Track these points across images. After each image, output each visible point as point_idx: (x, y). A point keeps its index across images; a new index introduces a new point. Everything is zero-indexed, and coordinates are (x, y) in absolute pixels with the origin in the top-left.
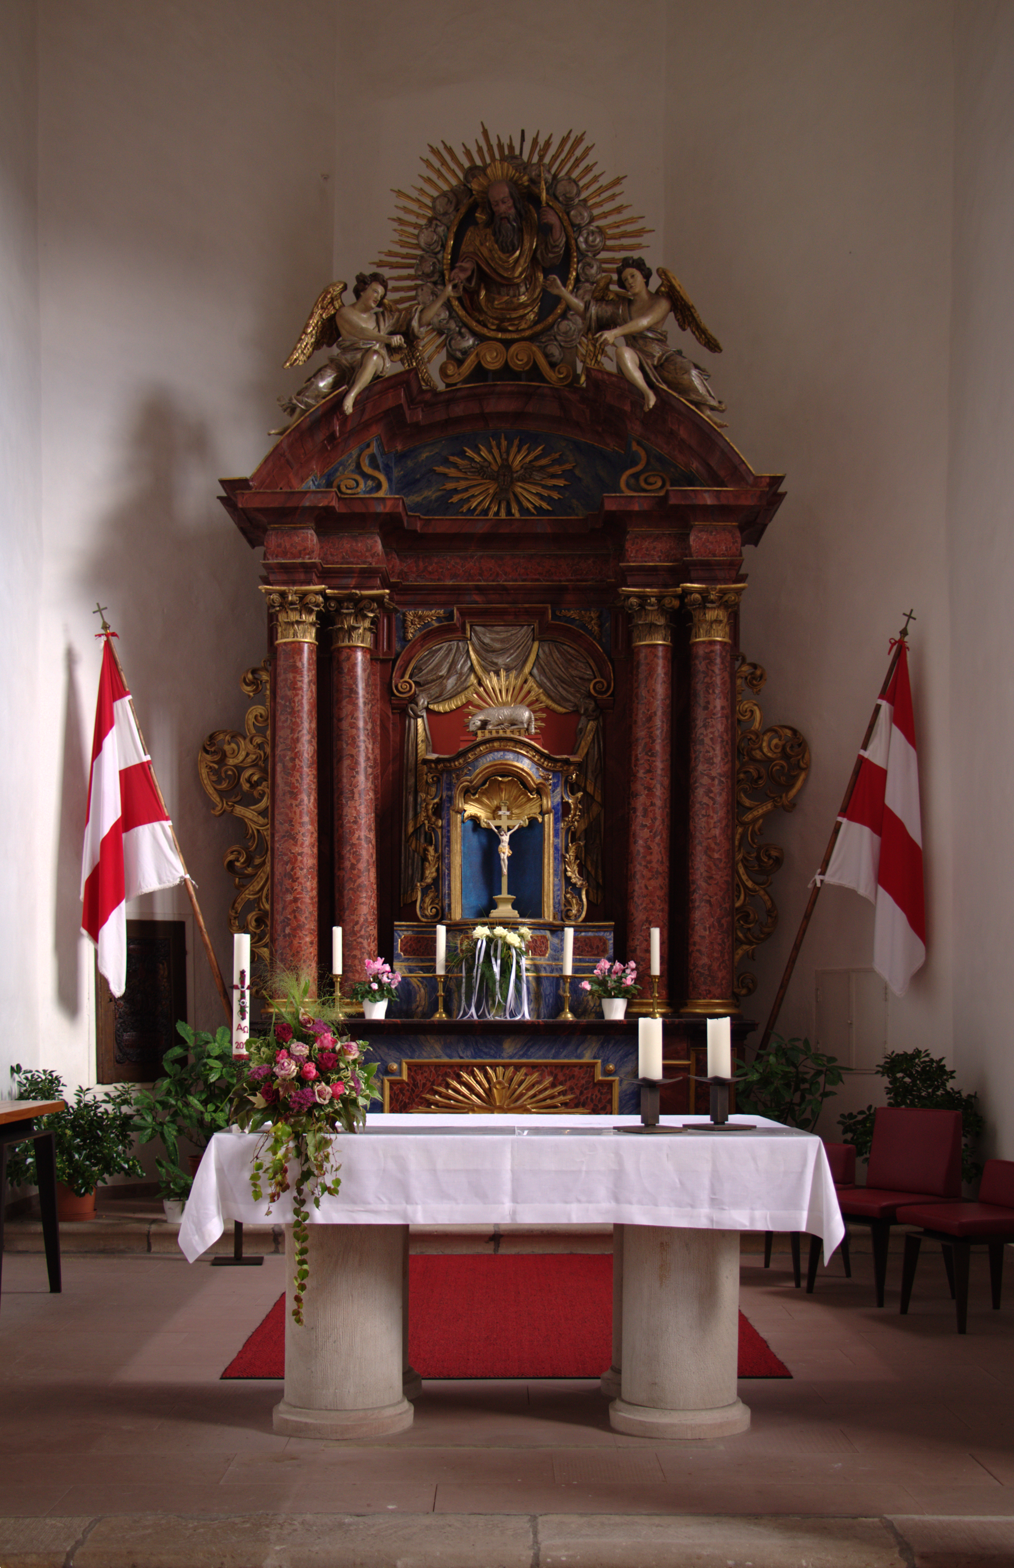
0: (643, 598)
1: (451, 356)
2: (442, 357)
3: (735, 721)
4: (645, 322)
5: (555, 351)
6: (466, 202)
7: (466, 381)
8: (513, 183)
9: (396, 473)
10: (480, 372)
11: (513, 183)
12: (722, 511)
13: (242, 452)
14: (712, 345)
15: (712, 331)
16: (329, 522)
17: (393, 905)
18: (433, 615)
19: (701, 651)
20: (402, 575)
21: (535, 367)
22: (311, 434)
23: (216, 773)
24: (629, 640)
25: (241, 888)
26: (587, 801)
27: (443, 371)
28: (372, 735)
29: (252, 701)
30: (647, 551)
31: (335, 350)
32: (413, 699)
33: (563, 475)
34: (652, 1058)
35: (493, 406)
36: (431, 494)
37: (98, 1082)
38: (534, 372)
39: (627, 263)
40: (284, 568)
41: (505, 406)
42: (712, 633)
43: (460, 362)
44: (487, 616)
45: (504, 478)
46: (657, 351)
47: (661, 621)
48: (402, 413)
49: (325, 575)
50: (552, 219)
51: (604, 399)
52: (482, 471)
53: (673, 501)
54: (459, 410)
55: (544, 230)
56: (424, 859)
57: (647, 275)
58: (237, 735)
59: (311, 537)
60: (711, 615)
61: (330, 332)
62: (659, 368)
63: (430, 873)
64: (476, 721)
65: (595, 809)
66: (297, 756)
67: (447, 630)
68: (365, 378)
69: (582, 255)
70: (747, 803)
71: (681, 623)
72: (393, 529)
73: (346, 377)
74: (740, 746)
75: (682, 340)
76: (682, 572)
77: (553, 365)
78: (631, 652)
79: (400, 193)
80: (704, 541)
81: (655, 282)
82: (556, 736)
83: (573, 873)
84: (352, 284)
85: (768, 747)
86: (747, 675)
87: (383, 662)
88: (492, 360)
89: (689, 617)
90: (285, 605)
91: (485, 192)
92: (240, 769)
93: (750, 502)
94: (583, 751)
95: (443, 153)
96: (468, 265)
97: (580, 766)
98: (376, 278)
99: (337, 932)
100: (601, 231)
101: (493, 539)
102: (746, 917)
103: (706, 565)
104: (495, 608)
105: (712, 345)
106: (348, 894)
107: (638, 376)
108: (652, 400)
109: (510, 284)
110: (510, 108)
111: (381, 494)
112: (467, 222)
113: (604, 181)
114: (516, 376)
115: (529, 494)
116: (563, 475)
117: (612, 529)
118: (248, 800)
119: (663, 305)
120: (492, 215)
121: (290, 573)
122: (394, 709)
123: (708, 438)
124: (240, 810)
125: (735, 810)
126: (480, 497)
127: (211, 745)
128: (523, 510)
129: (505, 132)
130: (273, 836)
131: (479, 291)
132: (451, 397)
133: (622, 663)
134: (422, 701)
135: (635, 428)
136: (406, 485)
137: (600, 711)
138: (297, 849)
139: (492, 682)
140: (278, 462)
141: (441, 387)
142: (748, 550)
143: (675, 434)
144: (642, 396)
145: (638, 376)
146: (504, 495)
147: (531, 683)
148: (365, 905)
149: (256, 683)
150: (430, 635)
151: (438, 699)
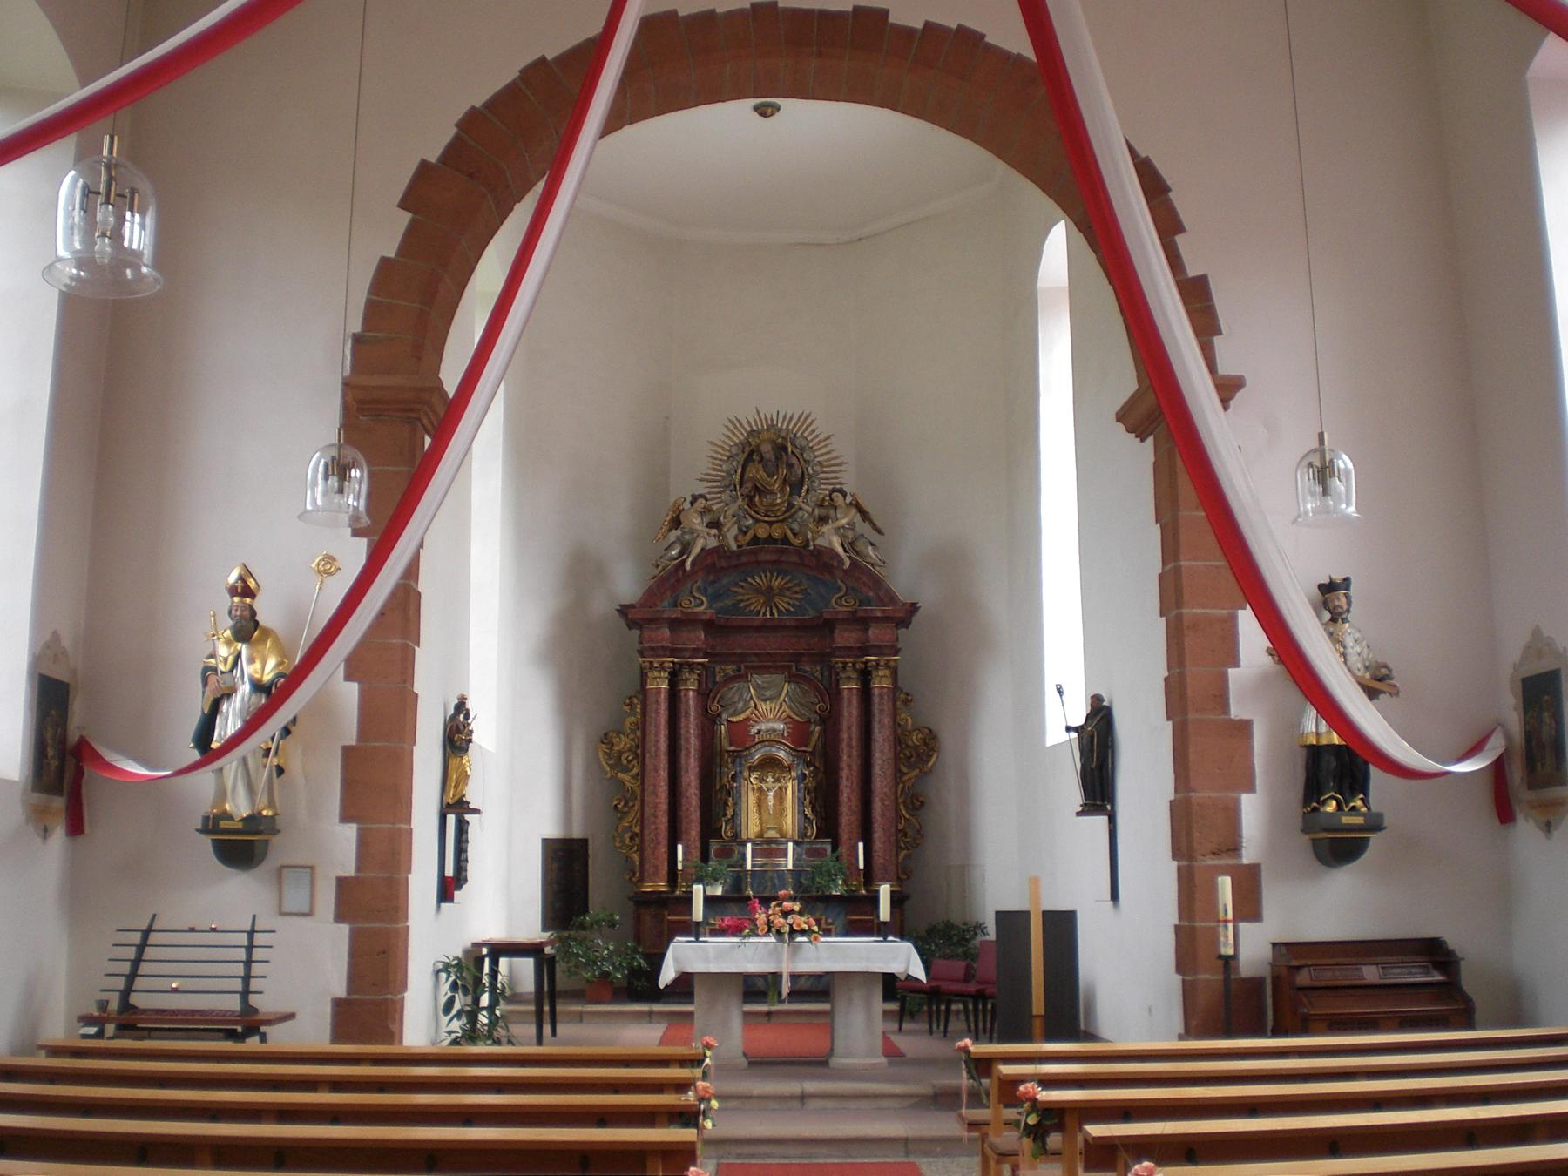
0: (845, 663)
1: (740, 530)
2: (735, 531)
3: (896, 723)
4: (844, 521)
5: (795, 526)
6: (747, 449)
7: (749, 544)
8: (773, 442)
9: (710, 590)
10: (756, 540)
11: (773, 442)
12: (887, 619)
13: (627, 584)
14: (879, 532)
15: (879, 524)
16: (675, 624)
17: (709, 830)
18: (730, 669)
19: (876, 692)
20: (713, 647)
21: (786, 536)
22: (669, 581)
23: (608, 755)
24: (837, 685)
25: (621, 819)
26: (815, 773)
27: (736, 538)
28: (698, 736)
29: (630, 715)
30: (845, 638)
31: (679, 532)
32: (719, 715)
33: (801, 592)
34: (885, 912)
35: (763, 557)
36: (729, 602)
37: (998, 913)
38: (785, 540)
39: (833, 491)
40: (652, 649)
41: (769, 557)
42: (880, 683)
43: (745, 533)
44: (760, 669)
45: (769, 594)
46: (850, 535)
47: (854, 675)
48: (714, 562)
49: (673, 652)
50: (794, 460)
51: (822, 561)
52: (757, 590)
53: (860, 614)
54: (744, 559)
55: (790, 466)
56: (726, 804)
57: (844, 495)
58: (619, 733)
59: (666, 632)
60: (881, 673)
61: (676, 522)
62: (852, 544)
63: (730, 813)
64: (754, 731)
65: (820, 775)
66: (658, 749)
67: (740, 676)
68: (696, 551)
69: (810, 477)
70: (905, 770)
71: (865, 676)
72: (709, 626)
73: (686, 548)
74: (899, 741)
75: (863, 527)
76: (865, 650)
77: (795, 535)
78: (839, 692)
79: (712, 443)
80: (875, 633)
81: (849, 499)
82: (798, 735)
83: (808, 812)
84: (689, 499)
85: (915, 739)
86: (900, 697)
87: (704, 695)
88: (762, 532)
89: (870, 673)
90: (652, 668)
91: (758, 446)
92: (621, 753)
93: (901, 615)
94: (813, 743)
95: (735, 423)
96: (749, 485)
97: (812, 753)
98: (702, 496)
99: (680, 847)
100: (820, 463)
101: (764, 628)
102: (905, 835)
103: (879, 647)
104: (768, 664)
105: (879, 532)
106: (684, 825)
107: (840, 550)
108: (847, 563)
109: (771, 492)
110: (771, 391)
111: (702, 608)
112: (748, 460)
113: (822, 437)
114: (775, 541)
115: (783, 604)
116: (801, 592)
117: (827, 626)
118: (626, 770)
119: (854, 511)
120: (762, 459)
121: (655, 652)
122: (709, 721)
123: (877, 582)
124: (621, 775)
125: (898, 775)
126: (757, 604)
127: (606, 739)
128: (780, 612)
129: (768, 410)
130: (643, 791)
131: (755, 493)
132: (738, 554)
133: (833, 694)
134: (724, 716)
135: (839, 574)
136: (714, 598)
137: (823, 721)
138: (956, 1024)
139: (763, 707)
140: (652, 595)
141: (734, 547)
142: (902, 631)
143: (864, 579)
144: (841, 561)
145: (840, 550)
146: (769, 602)
147: (785, 707)
148: (694, 831)
149: (631, 704)
150: (729, 680)
151: (734, 714)
